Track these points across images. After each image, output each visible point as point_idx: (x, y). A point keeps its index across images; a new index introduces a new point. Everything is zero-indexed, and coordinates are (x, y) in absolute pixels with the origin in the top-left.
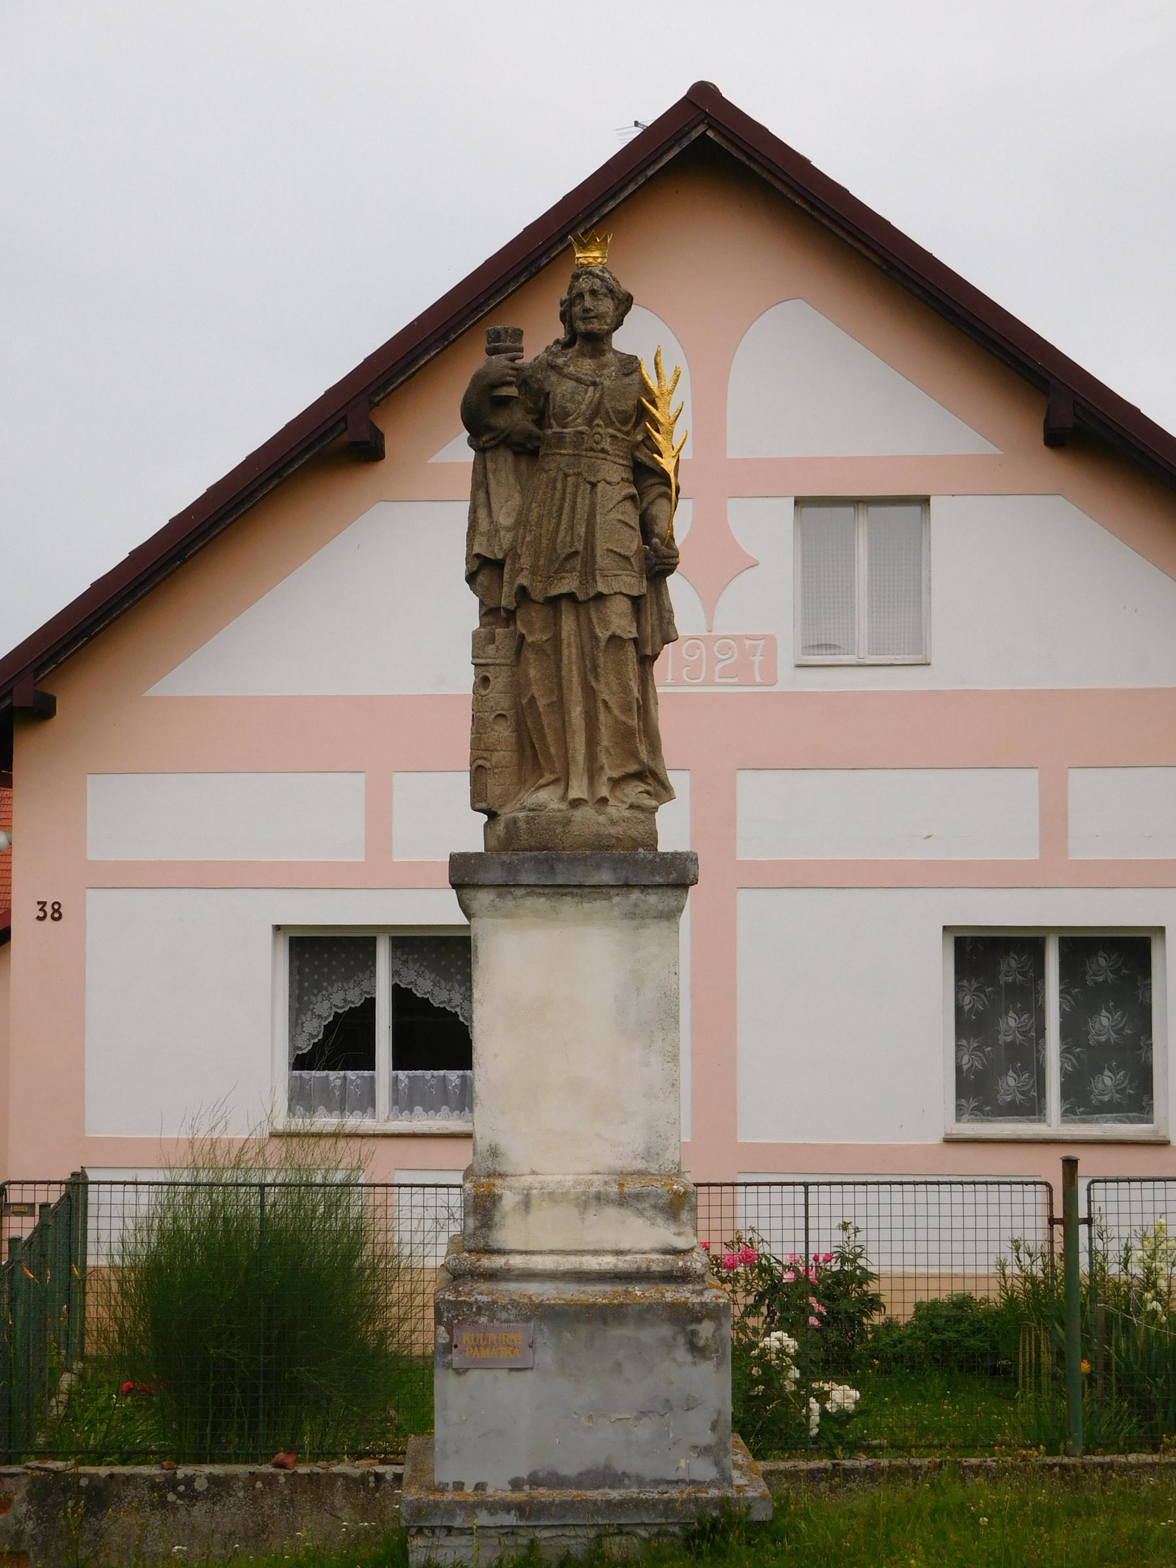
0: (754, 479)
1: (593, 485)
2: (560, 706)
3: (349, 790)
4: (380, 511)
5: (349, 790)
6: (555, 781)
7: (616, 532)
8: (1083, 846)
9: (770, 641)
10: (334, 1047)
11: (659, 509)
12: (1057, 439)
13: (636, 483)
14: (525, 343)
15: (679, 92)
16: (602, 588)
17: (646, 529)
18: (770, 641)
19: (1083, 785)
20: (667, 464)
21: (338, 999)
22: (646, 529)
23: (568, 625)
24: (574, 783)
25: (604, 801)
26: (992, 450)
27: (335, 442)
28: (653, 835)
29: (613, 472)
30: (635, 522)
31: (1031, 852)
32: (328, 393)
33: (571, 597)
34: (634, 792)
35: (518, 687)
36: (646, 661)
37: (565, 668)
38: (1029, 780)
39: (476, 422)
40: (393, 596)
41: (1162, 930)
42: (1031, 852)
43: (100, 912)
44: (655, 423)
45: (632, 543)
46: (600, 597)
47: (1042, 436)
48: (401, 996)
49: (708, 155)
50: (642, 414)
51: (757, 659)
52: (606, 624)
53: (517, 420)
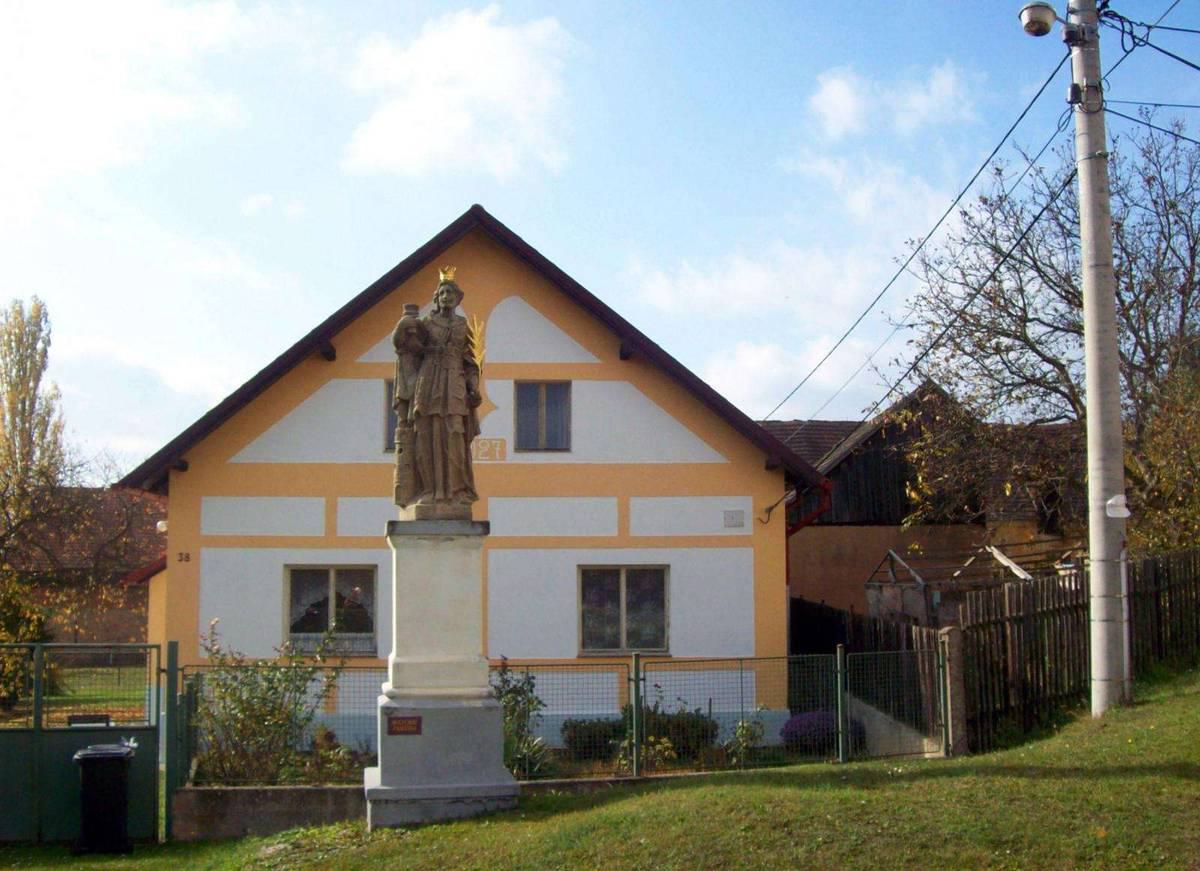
0: (501, 371)
1: (447, 370)
2: (432, 461)
3: (319, 503)
4: (334, 382)
5: (319, 503)
6: (430, 492)
7: (457, 392)
8: (636, 530)
9: (503, 442)
10: (306, 622)
11: (474, 380)
12: (625, 356)
13: (464, 369)
14: (421, 312)
15: (466, 208)
16: (450, 412)
17: (469, 388)
18: (503, 442)
19: (636, 504)
20: (478, 361)
21: (309, 599)
22: (469, 388)
23: (436, 425)
24: (437, 492)
25: (450, 500)
26: (597, 361)
27: (320, 348)
28: (471, 515)
29: (455, 365)
30: (464, 385)
31: (614, 533)
32: (314, 331)
33: (438, 415)
34: (463, 497)
35: (413, 453)
36: (468, 442)
37: (434, 443)
38: (614, 500)
39: (401, 345)
40: (352, 419)
41: (668, 566)
42: (614, 533)
43: (207, 555)
44: (472, 344)
45: (463, 394)
46: (450, 415)
47: (619, 355)
48: (340, 598)
49: (478, 233)
50: (468, 342)
51: (498, 449)
52: (452, 427)
53: (416, 343)
